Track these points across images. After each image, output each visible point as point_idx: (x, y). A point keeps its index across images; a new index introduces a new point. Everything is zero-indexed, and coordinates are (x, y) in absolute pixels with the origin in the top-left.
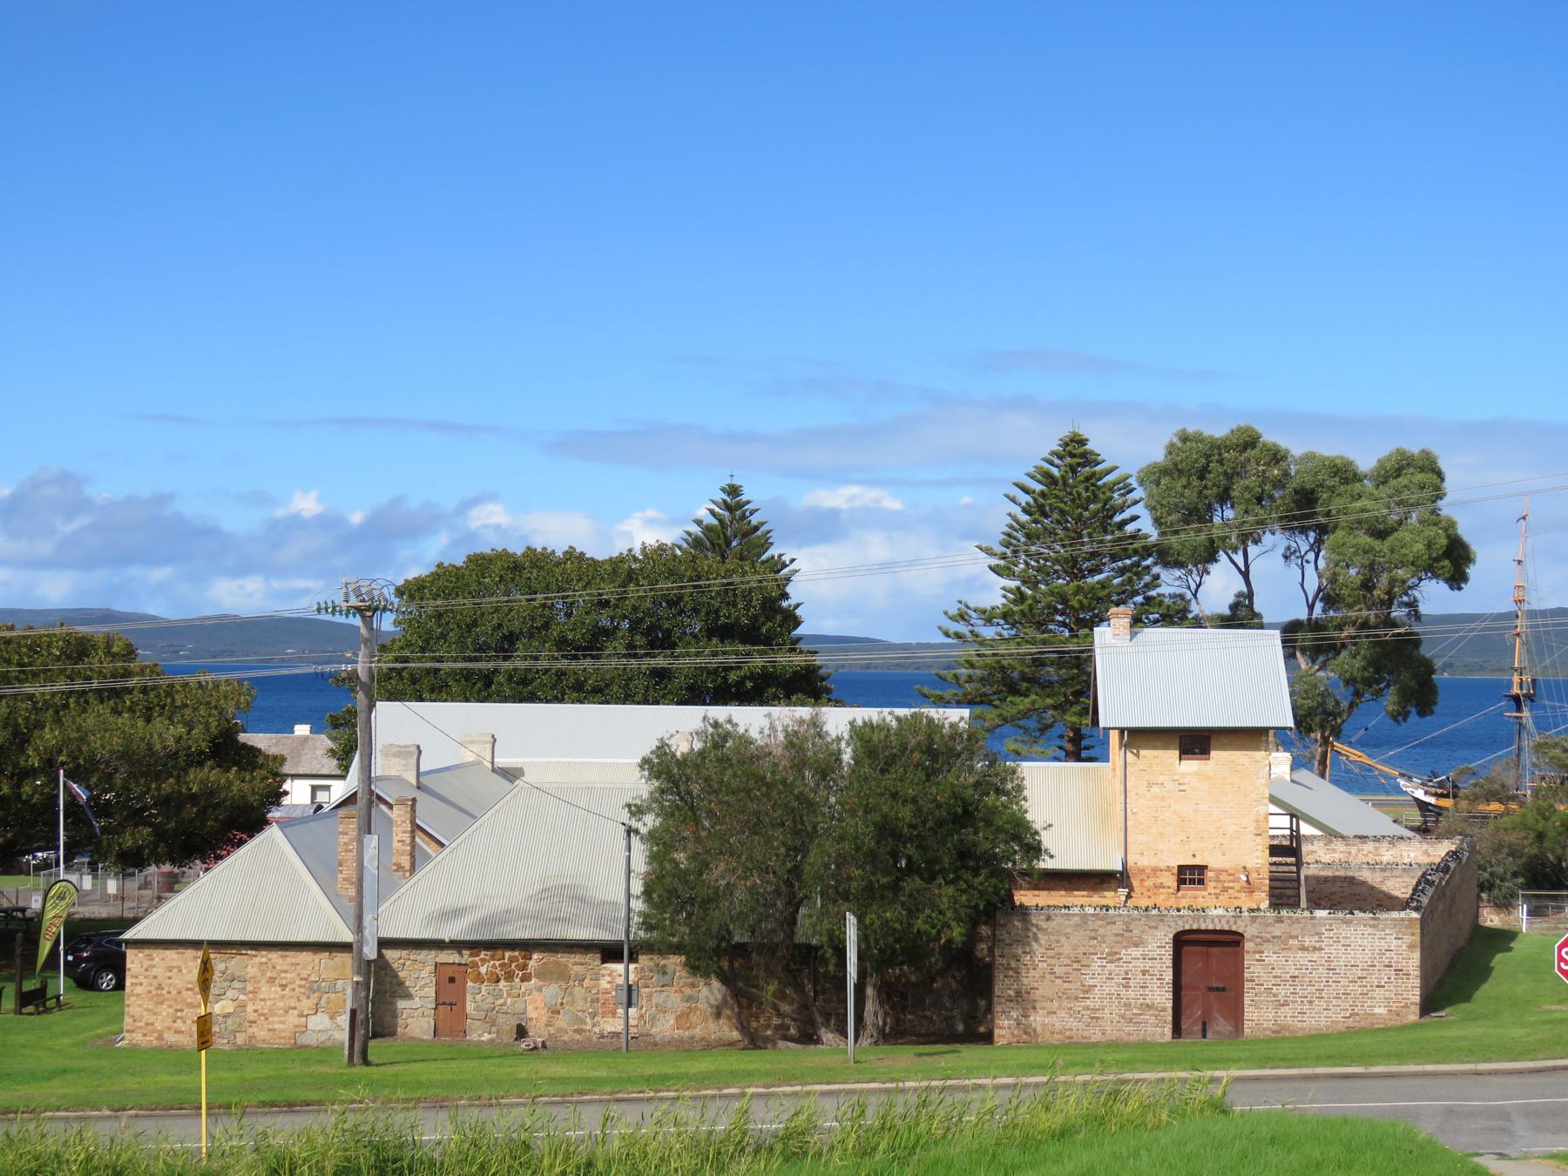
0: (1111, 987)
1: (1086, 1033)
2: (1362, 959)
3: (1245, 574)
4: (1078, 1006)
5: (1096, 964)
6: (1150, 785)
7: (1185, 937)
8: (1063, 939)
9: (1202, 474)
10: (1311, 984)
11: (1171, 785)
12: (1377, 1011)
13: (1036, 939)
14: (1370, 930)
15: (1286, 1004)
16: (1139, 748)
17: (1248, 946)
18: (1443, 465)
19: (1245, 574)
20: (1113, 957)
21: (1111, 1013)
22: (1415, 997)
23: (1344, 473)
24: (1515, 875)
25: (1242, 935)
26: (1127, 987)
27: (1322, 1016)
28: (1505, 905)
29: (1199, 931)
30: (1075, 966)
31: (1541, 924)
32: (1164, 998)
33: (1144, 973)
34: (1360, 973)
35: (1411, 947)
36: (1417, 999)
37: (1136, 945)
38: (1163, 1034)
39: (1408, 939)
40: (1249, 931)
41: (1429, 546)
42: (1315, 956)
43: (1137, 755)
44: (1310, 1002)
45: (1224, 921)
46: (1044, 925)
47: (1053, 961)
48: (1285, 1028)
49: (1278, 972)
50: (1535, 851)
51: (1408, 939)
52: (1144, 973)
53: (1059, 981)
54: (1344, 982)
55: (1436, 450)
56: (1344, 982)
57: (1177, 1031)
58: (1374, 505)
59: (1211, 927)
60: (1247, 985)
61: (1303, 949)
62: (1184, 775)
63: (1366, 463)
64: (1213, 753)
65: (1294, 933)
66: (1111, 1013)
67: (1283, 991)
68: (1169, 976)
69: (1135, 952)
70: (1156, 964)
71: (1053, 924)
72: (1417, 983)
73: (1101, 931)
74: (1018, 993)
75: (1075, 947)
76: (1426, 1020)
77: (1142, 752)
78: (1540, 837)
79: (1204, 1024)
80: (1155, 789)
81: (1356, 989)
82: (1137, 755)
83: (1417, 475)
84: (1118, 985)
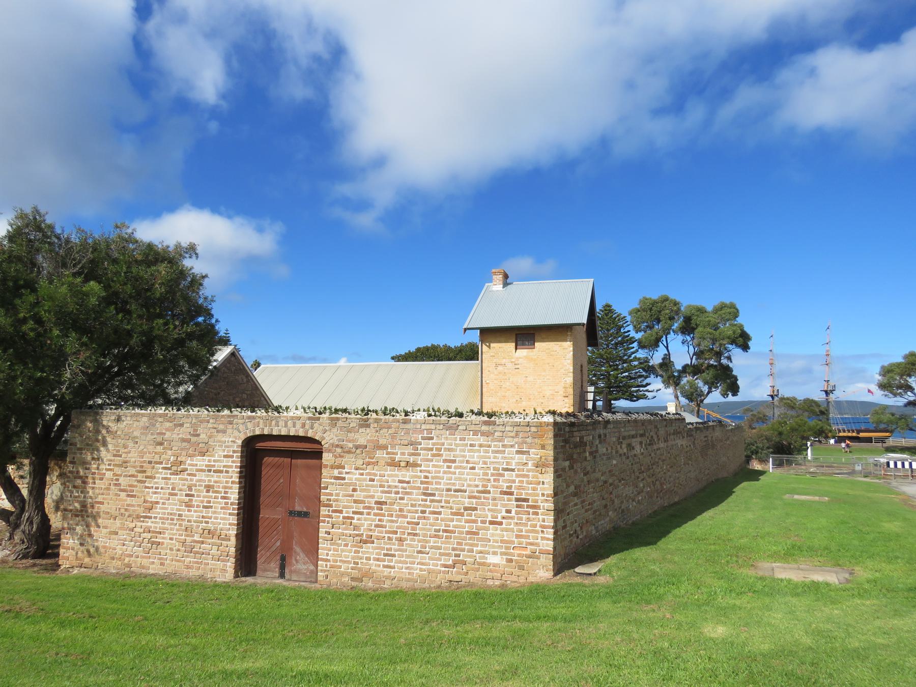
0: (173, 506)
1: (145, 562)
2: (470, 480)
3: (667, 348)
4: (139, 526)
5: (161, 474)
6: (497, 365)
7: (260, 445)
8: (131, 444)
9: (651, 309)
10: (401, 514)
11: (510, 365)
12: (492, 559)
13: (105, 444)
14: (482, 440)
15: (369, 540)
16: (490, 342)
17: (327, 457)
18: (738, 307)
19: (667, 348)
20: (177, 468)
21: (171, 537)
22: (546, 542)
23: (701, 311)
24: (768, 448)
25: (319, 443)
26: (189, 505)
27: (414, 563)
28: (763, 461)
29: (270, 437)
30: (140, 477)
31: (779, 471)
32: (227, 522)
33: (208, 488)
34: (467, 502)
35: (540, 465)
36: (549, 545)
37: (203, 454)
38: (224, 571)
39: (536, 454)
40: (328, 436)
41: (734, 333)
42: (407, 474)
43: (489, 347)
44: (400, 540)
45: (299, 424)
46: (113, 426)
47: (118, 470)
48: (369, 574)
49: (359, 495)
50: (778, 439)
51: (536, 454)
52: (208, 488)
53: (123, 494)
54: (446, 513)
55: (735, 302)
56: (446, 513)
57: (246, 562)
58: (713, 319)
59: (301, 434)
60: (324, 511)
61: (394, 464)
62: (518, 359)
63: (709, 308)
64: (536, 344)
65: (382, 441)
66: (171, 537)
67: (365, 523)
68: (234, 495)
69: (201, 462)
70: (222, 478)
71: (122, 425)
72: (550, 519)
73: (168, 434)
74: (84, 506)
75: (142, 454)
76: (568, 578)
77: (492, 345)
78: (780, 434)
79: (283, 559)
80: (500, 368)
81: (461, 524)
82: (489, 347)
83: (729, 312)
84: (181, 502)
